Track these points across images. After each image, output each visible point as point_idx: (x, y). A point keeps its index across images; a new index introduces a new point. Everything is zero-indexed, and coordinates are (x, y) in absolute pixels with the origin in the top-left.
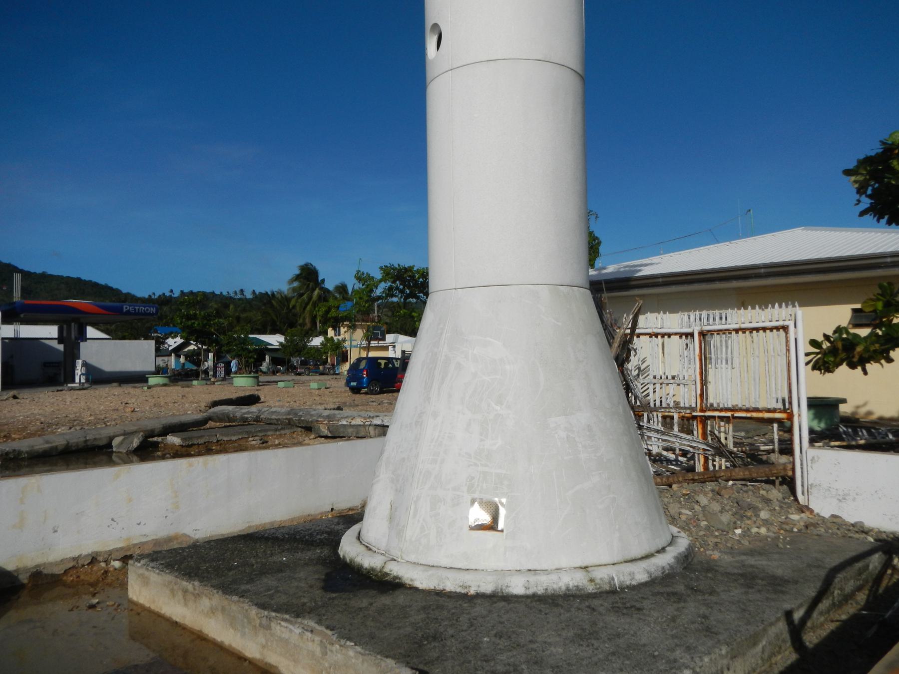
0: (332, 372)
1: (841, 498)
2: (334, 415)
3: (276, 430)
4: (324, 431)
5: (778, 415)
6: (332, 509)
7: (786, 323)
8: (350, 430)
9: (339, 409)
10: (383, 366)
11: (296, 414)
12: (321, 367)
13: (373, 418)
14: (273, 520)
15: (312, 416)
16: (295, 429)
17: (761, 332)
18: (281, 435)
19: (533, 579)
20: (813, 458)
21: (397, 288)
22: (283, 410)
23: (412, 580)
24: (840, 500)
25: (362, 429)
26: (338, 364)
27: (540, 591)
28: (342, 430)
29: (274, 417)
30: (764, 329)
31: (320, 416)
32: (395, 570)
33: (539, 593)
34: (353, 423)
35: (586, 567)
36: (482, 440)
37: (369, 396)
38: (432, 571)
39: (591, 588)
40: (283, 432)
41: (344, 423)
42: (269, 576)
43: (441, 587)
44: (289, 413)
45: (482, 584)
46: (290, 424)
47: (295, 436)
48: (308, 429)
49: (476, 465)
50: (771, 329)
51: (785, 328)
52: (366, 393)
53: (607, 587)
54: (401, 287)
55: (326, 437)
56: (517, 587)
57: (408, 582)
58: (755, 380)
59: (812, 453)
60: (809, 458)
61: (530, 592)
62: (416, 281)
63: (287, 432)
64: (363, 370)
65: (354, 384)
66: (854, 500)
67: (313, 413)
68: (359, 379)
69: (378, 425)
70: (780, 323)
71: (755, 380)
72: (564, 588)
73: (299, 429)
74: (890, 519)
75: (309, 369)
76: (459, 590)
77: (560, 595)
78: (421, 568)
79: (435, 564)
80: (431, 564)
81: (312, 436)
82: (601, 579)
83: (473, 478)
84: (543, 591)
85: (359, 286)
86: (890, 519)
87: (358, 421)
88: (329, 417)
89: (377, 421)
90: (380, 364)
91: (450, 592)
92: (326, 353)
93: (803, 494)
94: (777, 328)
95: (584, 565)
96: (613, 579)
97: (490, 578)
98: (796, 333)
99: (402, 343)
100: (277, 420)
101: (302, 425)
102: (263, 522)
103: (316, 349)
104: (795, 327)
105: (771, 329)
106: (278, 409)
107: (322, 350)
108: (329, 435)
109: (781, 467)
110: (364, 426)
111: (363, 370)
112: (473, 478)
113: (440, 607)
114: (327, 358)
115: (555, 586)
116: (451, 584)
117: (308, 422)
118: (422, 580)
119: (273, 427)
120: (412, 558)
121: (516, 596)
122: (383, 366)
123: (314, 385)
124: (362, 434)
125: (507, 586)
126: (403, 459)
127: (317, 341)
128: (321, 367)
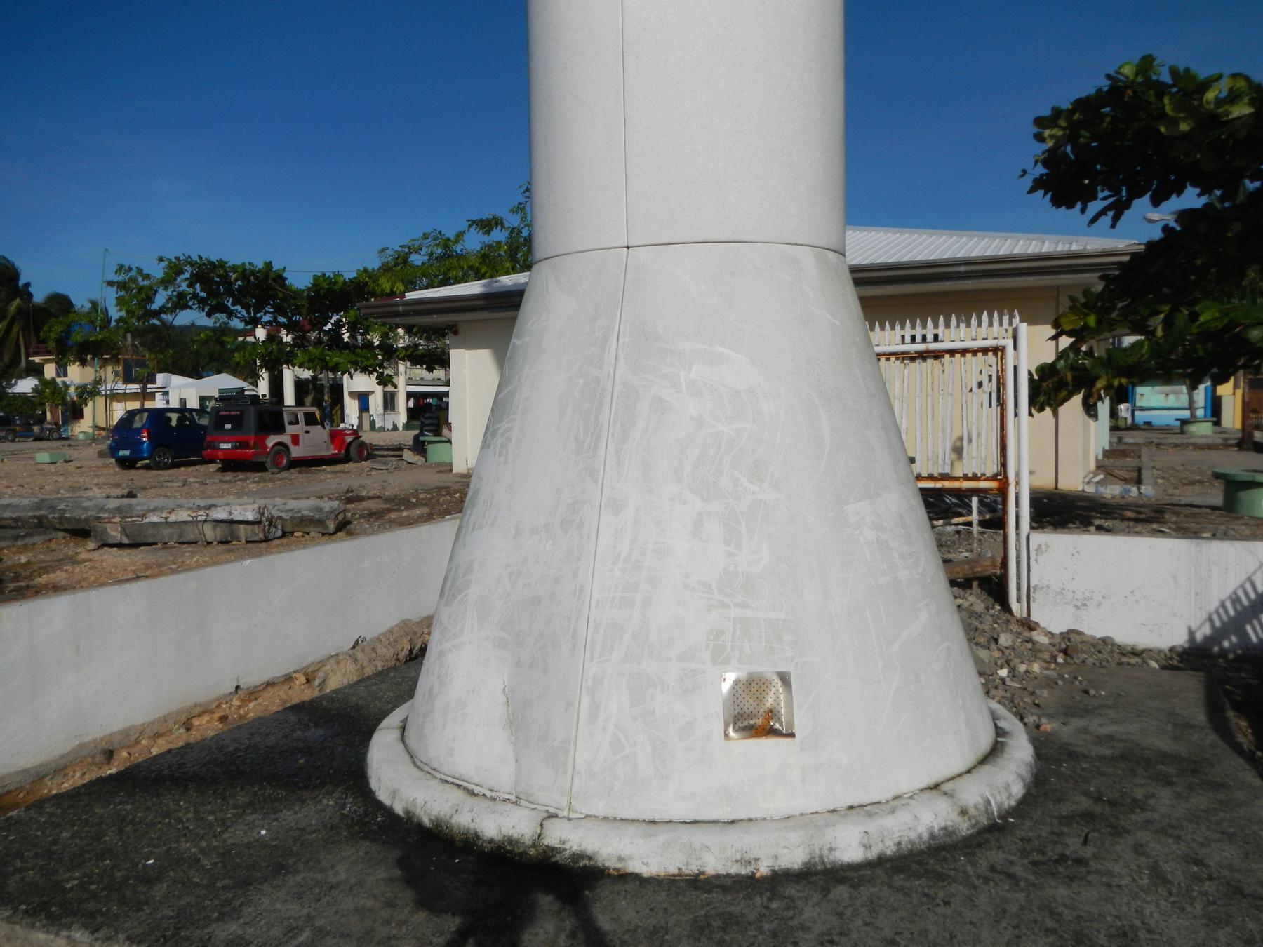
0: (55, 435)
1: (1079, 604)
2: (130, 506)
3: (16, 538)
4: (115, 534)
5: (983, 484)
6: (237, 687)
7: (1001, 342)
8: (166, 532)
9: (131, 495)
10: (174, 423)
11: (52, 508)
12: (36, 429)
13: (209, 507)
14: (128, 724)
15: (85, 509)
16: (53, 534)
17: (958, 356)
18: (25, 546)
19: (873, 826)
20: (1040, 546)
21: (195, 296)
22: (26, 502)
23: (621, 859)
24: (1077, 608)
25: (189, 528)
26: (66, 422)
27: (889, 848)
28: (150, 531)
29: (7, 515)
30: (963, 352)
31: (102, 509)
32: (570, 838)
33: (889, 852)
34: (172, 518)
35: (936, 787)
36: (729, 555)
37: (154, 472)
38: (663, 836)
39: (965, 828)
40: (29, 541)
41: (155, 518)
42: (266, 888)
43: (693, 868)
44: (38, 506)
45: (782, 851)
46: (41, 525)
47: (53, 545)
48: (81, 532)
49: (723, 605)
50: (974, 352)
51: (998, 351)
52: (147, 467)
53: (984, 821)
54: (203, 294)
55: (120, 546)
56: (849, 846)
57: (612, 863)
58: (943, 431)
59: (1039, 538)
60: (1033, 546)
61: (872, 854)
62: (230, 284)
63: (38, 539)
64: (139, 431)
65: (124, 453)
66: (1099, 605)
67: (87, 504)
68: (135, 445)
69: (222, 521)
70: (990, 343)
71: (943, 431)
72: (925, 836)
73: (61, 534)
74: (1151, 631)
75: (14, 431)
76: (734, 870)
77: (921, 852)
78: (632, 829)
79: (657, 817)
80: (647, 817)
81: (91, 545)
82: (975, 806)
83: (720, 633)
84: (894, 849)
85: (1109, 83)
86: (1151, 631)
87: (183, 516)
88: (119, 510)
89: (220, 514)
90: (170, 419)
91: (717, 877)
92: (42, 404)
93: (1019, 600)
94: (985, 351)
95: (932, 782)
96: (988, 802)
97: (795, 837)
98: (1017, 358)
99: (180, 388)
100: (16, 520)
101: (66, 526)
102: (108, 732)
103: (22, 396)
104: (1015, 348)
105: (974, 352)
106: (16, 501)
107: (37, 401)
108: (126, 541)
109: (988, 563)
110: (194, 523)
111: (139, 431)
112: (720, 633)
113: (730, 921)
114: (44, 413)
115: (913, 835)
116: (715, 857)
117: (79, 521)
118: (648, 857)
119: (10, 532)
120: (599, 808)
121: (851, 867)
122: (174, 423)
123: (43, 457)
124: (191, 537)
125: (831, 849)
126: (536, 601)
127: (25, 386)
128: (36, 429)
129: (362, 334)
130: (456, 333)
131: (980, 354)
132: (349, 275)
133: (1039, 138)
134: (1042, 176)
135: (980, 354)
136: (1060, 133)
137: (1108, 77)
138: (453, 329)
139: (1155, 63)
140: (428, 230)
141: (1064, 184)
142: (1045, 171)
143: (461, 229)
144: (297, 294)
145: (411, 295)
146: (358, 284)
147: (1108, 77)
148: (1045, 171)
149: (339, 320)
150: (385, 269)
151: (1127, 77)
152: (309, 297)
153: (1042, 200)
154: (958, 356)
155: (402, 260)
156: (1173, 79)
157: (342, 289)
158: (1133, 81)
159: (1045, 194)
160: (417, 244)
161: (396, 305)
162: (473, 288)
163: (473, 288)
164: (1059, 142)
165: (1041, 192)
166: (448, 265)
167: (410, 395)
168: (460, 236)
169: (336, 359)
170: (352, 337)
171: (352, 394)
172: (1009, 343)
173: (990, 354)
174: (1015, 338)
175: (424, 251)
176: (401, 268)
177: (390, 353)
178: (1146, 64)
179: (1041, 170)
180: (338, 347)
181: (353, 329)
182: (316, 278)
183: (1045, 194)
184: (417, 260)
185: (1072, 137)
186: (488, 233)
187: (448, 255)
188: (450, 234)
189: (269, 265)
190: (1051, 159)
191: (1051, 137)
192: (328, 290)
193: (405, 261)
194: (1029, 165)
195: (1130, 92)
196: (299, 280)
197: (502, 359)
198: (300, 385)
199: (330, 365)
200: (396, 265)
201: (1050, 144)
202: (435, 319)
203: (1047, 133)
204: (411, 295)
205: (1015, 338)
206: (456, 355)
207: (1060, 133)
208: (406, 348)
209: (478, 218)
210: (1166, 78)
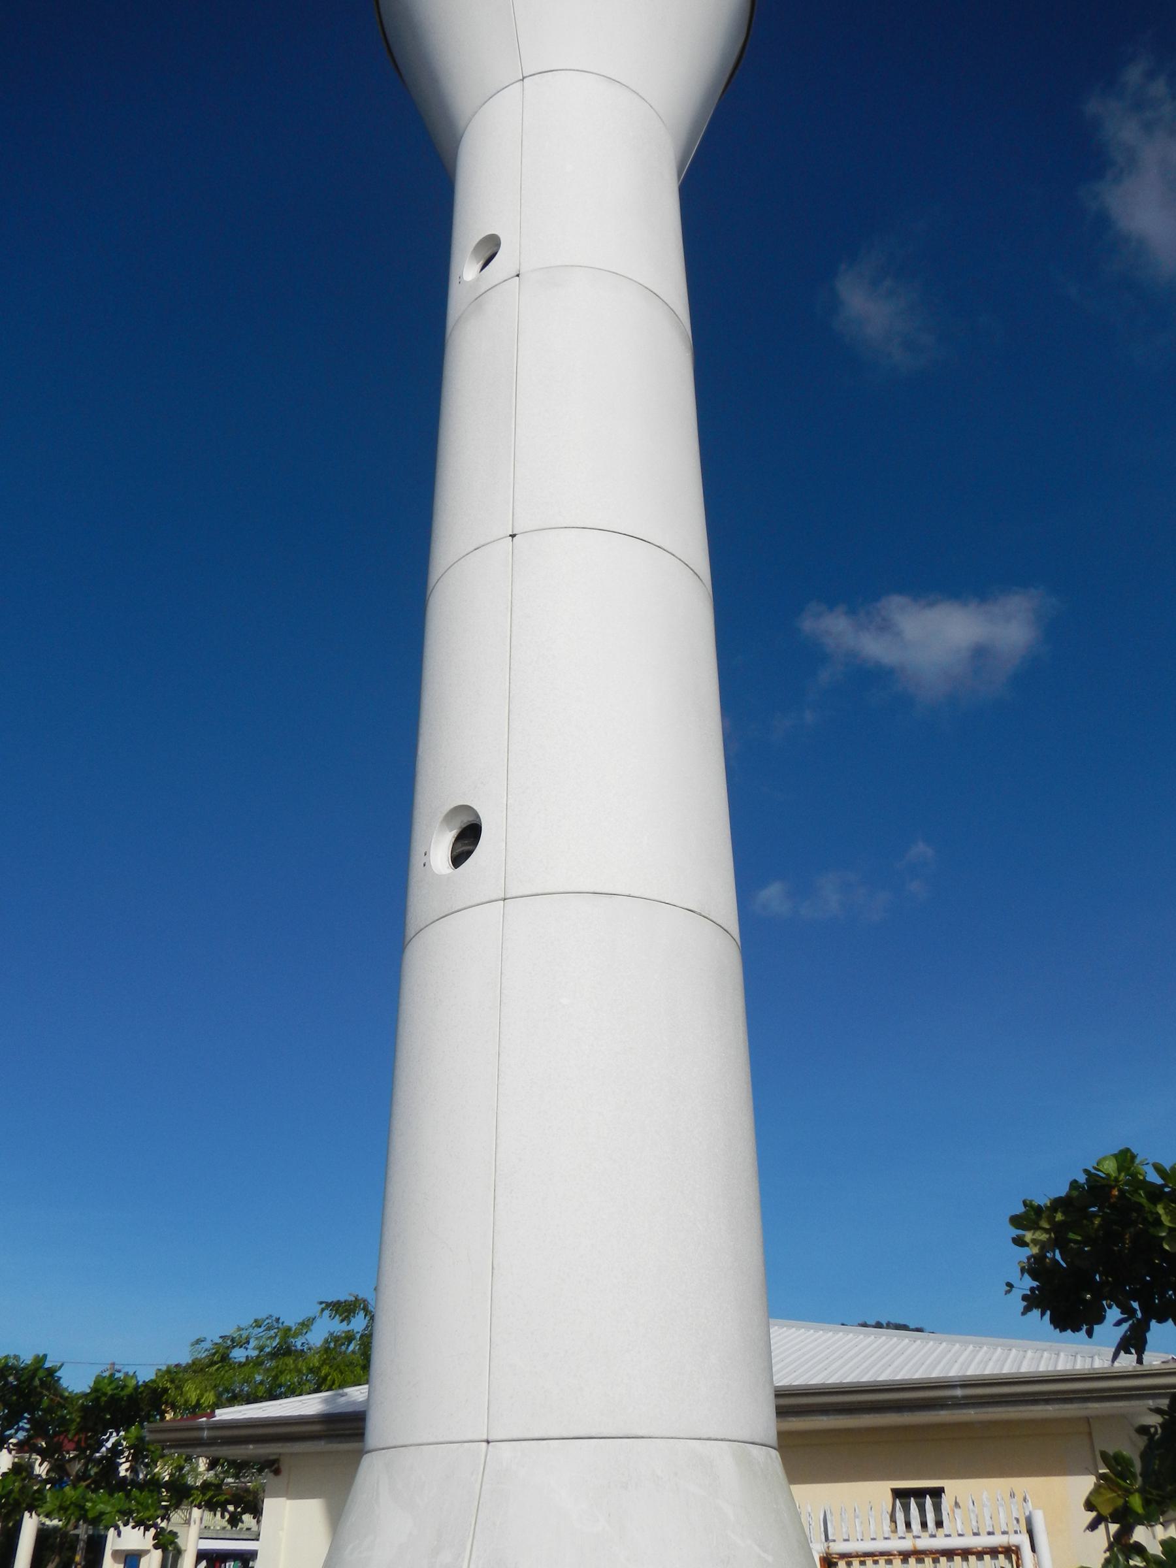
7: (1014, 1540)
17: (958, 1559)
30: (965, 1553)
50: (980, 1555)
94: (994, 1552)
104: (1033, 1549)
105: (980, 1555)
129: (147, 1465)
130: (277, 1472)
131: (987, 1557)
132: (146, 1375)
133: (1019, 1242)
134: (1032, 1289)
135: (987, 1557)
136: (1044, 1237)
137: (1086, 1171)
138: (272, 1466)
139: (1137, 1161)
140: (262, 1315)
141: (1063, 1299)
142: (1035, 1284)
143: (311, 1315)
144: (66, 1400)
145: (225, 1414)
146: (154, 1390)
147: (1086, 1171)
148: (1035, 1284)
149: (117, 1444)
150: (197, 1368)
151: (1108, 1175)
152: (84, 1408)
153: (1039, 1321)
154: (958, 1559)
155: (221, 1356)
156: (1163, 1178)
157: (130, 1397)
158: (1116, 1180)
159: (1043, 1314)
160: (245, 1334)
161: (200, 1428)
162: (309, 1405)
163: (309, 1405)
164: (1044, 1247)
165: (1036, 1313)
166: (284, 1366)
167: (201, 1555)
168: (306, 1325)
169: (101, 1507)
170: (133, 1469)
171: (116, 1554)
172: (1023, 1540)
173: (1001, 1557)
174: (1030, 1532)
175: (253, 1343)
176: (221, 1372)
177: (180, 1493)
178: (1125, 1158)
179: (1028, 1283)
180: (108, 1484)
181: (139, 1452)
182: (99, 1380)
183: (1043, 1314)
184: (239, 1355)
185: (1059, 1241)
186: (346, 1319)
187: (284, 1351)
188: (291, 1321)
189: (40, 1360)
190: (1036, 1268)
191: (1035, 1242)
192: (112, 1396)
193: (225, 1358)
194: (1014, 1275)
195: (1115, 1192)
196: (76, 1381)
197: (336, 1516)
198: (43, 1536)
199: (90, 1515)
200: (213, 1363)
201: (1035, 1250)
202: (251, 1450)
203: (1029, 1236)
204: (225, 1414)
205: (1030, 1532)
206: (270, 1505)
207: (1044, 1237)
208: (206, 1486)
209: (335, 1300)
210: (1154, 1178)
